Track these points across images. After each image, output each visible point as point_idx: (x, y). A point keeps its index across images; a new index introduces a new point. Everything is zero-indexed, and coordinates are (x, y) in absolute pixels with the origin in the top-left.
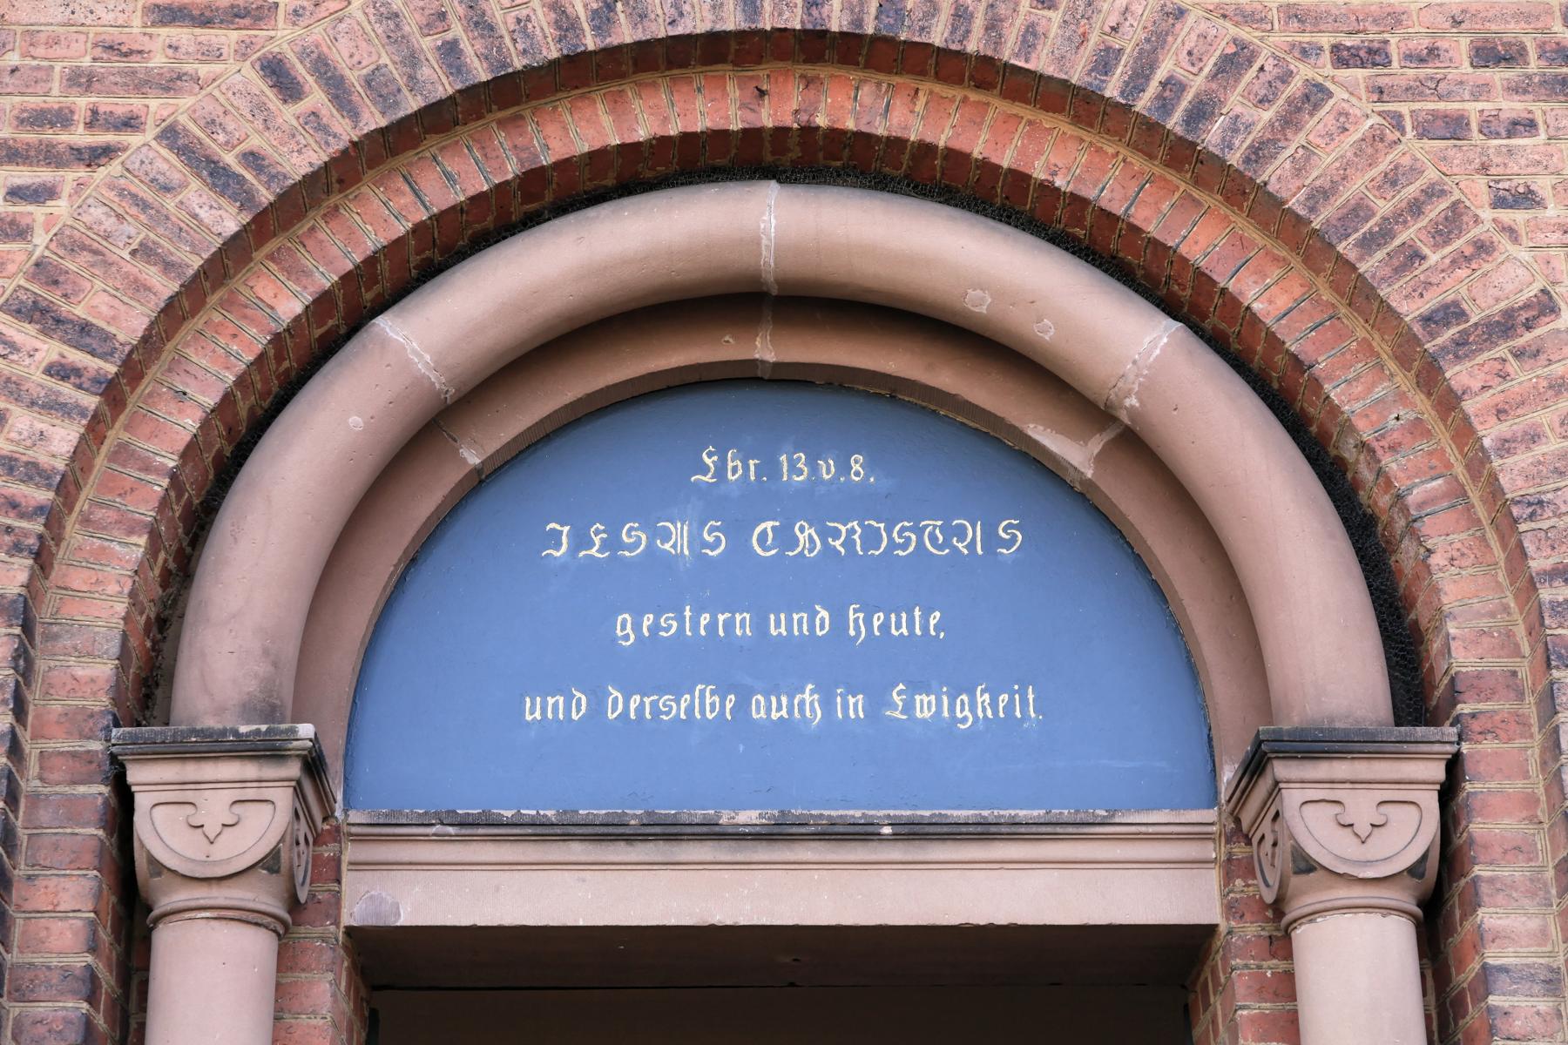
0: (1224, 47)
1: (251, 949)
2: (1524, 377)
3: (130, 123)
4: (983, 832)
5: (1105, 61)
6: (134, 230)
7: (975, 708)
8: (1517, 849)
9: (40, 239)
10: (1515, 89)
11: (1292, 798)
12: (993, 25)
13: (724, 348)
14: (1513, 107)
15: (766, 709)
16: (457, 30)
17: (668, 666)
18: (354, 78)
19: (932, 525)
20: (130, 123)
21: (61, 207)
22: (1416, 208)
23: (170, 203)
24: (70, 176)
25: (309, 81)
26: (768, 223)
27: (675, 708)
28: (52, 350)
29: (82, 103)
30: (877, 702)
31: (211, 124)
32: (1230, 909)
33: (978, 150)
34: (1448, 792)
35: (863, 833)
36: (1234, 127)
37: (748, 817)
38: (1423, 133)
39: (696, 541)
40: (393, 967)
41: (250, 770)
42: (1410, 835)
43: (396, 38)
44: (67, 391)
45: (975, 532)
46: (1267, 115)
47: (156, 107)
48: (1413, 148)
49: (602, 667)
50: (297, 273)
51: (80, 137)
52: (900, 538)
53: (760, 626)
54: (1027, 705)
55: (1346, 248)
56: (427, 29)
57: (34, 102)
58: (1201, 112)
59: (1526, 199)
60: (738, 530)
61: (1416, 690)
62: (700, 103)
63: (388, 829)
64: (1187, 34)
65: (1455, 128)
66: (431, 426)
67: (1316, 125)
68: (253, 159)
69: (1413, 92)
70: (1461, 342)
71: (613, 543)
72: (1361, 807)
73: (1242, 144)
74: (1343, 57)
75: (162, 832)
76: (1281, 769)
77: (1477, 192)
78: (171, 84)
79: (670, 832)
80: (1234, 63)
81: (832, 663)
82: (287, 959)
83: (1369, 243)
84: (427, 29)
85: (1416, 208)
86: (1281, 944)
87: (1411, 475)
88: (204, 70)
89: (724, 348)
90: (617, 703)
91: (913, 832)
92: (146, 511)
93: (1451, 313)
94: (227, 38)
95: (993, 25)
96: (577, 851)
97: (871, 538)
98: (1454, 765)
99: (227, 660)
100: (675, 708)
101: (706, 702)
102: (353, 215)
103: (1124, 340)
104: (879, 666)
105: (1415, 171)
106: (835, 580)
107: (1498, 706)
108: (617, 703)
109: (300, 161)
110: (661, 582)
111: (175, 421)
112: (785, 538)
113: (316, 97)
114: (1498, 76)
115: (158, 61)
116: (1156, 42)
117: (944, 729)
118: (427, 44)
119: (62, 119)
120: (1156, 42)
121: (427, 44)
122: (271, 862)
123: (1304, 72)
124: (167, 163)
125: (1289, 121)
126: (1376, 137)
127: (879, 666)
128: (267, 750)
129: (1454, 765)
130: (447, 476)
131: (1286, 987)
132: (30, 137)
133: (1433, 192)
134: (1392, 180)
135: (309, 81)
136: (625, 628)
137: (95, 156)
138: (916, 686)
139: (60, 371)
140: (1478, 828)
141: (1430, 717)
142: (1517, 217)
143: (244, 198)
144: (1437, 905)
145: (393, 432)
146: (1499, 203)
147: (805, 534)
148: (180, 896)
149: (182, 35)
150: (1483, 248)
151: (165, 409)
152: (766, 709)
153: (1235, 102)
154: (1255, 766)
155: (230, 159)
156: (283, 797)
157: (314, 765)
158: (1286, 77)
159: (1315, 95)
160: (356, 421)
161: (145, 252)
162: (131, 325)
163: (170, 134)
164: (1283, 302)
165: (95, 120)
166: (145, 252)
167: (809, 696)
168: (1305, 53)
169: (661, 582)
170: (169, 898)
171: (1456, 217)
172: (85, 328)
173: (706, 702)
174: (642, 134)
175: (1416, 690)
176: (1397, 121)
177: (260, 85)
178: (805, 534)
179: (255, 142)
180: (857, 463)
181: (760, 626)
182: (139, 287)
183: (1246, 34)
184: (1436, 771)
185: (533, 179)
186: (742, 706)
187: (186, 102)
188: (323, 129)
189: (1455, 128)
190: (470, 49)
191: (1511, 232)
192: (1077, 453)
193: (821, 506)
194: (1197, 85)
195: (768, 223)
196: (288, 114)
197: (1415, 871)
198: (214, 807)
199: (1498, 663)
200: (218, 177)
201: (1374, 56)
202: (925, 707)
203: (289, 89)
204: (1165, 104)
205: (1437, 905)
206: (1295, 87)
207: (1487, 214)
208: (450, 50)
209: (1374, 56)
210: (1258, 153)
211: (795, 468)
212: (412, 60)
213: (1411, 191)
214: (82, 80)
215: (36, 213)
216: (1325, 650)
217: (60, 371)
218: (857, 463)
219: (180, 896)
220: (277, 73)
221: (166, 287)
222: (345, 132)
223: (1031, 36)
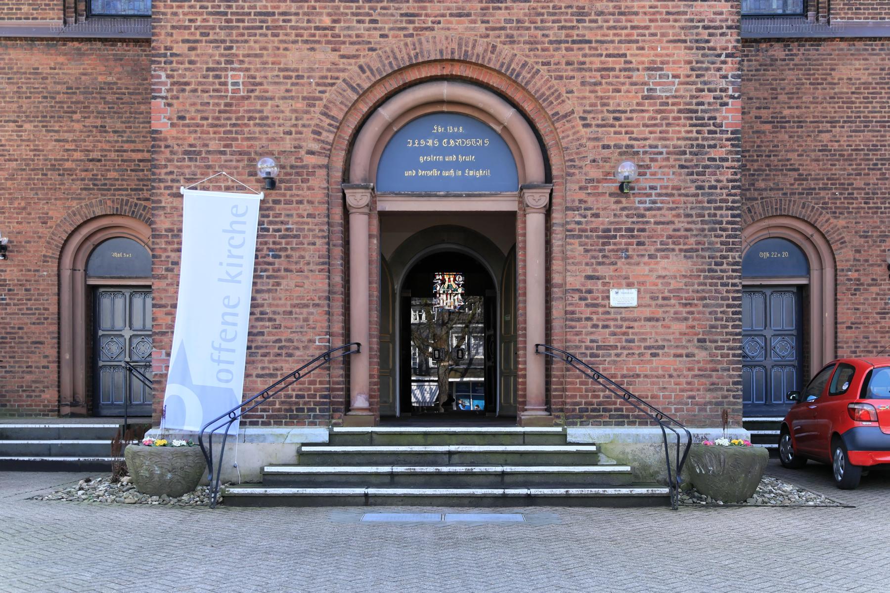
0: (523, 62)
1: (365, 218)
2: (568, 125)
3: (337, 78)
4: (480, 196)
5: (502, 65)
6: (340, 99)
7: (480, 173)
8: (560, 204)
9: (325, 100)
10: (572, 70)
11: (526, 195)
12: (483, 58)
13: (438, 108)
14: (571, 74)
15: (446, 174)
16: (391, 59)
17: (428, 166)
18: (374, 69)
19: (473, 140)
20: (337, 78)
21: (327, 94)
22: (553, 94)
23: (345, 94)
24: (329, 88)
25: (367, 69)
26: (445, 90)
27: (430, 173)
28: (328, 121)
29: (329, 74)
30: (463, 172)
31: (351, 78)
32: (520, 209)
33: (481, 79)
34: (551, 194)
35: (460, 196)
36: (524, 78)
37: (442, 193)
38: (556, 79)
39: (433, 143)
40: (384, 216)
41: (363, 191)
42: (545, 201)
43: (381, 61)
44: (331, 128)
45: (481, 141)
46: (529, 76)
47: (341, 75)
48: (554, 82)
49: (418, 166)
50: (366, 103)
51: (330, 81)
52: (468, 142)
53: (444, 159)
54: (488, 173)
55: (540, 101)
56: (386, 59)
57: (321, 74)
58: (518, 75)
59: (572, 92)
60: (440, 142)
61: (548, 178)
62: (433, 70)
63: (384, 195)
64: (516, 60)
65: (561, 78)
66: (389, 126)
67: (538, 77)
68: (358, 85)
69: (555, 71)
70: (558, 119)
71: (419, 144)
72: (537, 196)
73: (525, 81)
74: (544, 64)
75: (350, 200)
76: (524, 191)
77: (563, 90)
78: (344, 70)
79: (429, 196)
80: (524, 65)
81: (456, 165)
82: (369, 218)
83: (544, 101)
84: (386, 59)
85: (553, 94)
86: (525, 215)
87: (548, 140)
88: (349, 68)
89: (438, 108)
90: (421, 173)
91: (468, 196)
92: (344, 147)
93: (557, 113)
94: (352, 61)
95: (483, 58)
96: (414, 198)
97: (463, 143)
98: (552, 190)
99: (358, 171)
100: (430, 173)
101: (435, 172)
102: (375, 92)
103: (506, 113)
104: (463, 166)
105: (553, 86)
106: (456, 150)
107: (560, 180)
108: (421, 173)
109: (366, 85)
110: (427, 151)
111: (349, 131)
112: (448, 143)
113: (368, 73)
114: (569, 67)
115: (341, 66)
116: (512, 61)
117: (474, 177)
118: (386, 62)
119: (326, 77)
120: (512, 61)
121: (386, 62)
122: (367, 205)
123: (536, 67)
124: (344, 86)
125: (533, 77)
126: (547, 80)
127: (463, 166)
128: (366, 188)
129: (552, 190)
130: (392, 134)
131: (525, 222)
132: (321, 81)
133: (556, 90)
134: (549, 88)
135: (367, 69)
136: (421, 159)
137: (333, 84)
138: (470, 170)
139: (330, 125)
140: (554, 201)
141: (550, 182)
142: (570, 95)
143: (357, 93)
144: (548, 212)
145: (383, 129)
146: (567, 93)
147: (452, 142)
148: (354, 210)
149: (345, 60)
150: (563, 101)
151: (346, 129)
152: (446, 174)
153: (524, 73)
154: (522, 189)
155: (354, 85)
156: (369, 195)
157: (373, 189)
158: (533, 68)
159: (538, 71)
160: (377, 129)
161: (342, 103)
162: (340, 116)
163: (344, 80)
164: (531, 108)
165: (332, 78)
166: (342, 103)
167: (452, 171)
168: (537, 63)
169: (427, 151)
170: (351, 211)
171: (559, 96)
172: (333, 117)
173: (435, 172)
174: (423, 76)
175: (548, 178)
176: (551, 77)
177: (359, 71)
178: (452, 142)
179: (358, 82)
180: (461, 128)
181: (444, 159)
182: (341, 109)
183: (527, 59)
184: (549, 191)
185: (405, 84)
186: (441, 173)
187: (346, 74)
188: (370, 79)
189: (561, 78)
190: (394, 63)
191: (568, 98)
192: (498, 129)
193: (455, 136)
194: (518, 69)
195: (445, 90)
196: (364, 76)
197: (545, 206)
198: (358, 196)
199: (560, 173)
200: (353, 89)
201: (548, 64)
202: (471, 173)
203: (363, 71)
204: (512, 74)
205: (548, 212)
206: (534, 70)
207: (565, 95)
208: (390, 63)
209: (548, 64)
210: (527, 83)
211: (450, 129)
212: (384, 65)
213: (552, 90)
214: (329, 70)
215: (324, 95)
216: (534, 170)
217: (330, 125)
218: (461, 128)
219: (354, 210)
220: (361, 67)
221: (346, 109)
222: (374, 80)
223: (490, 60)
